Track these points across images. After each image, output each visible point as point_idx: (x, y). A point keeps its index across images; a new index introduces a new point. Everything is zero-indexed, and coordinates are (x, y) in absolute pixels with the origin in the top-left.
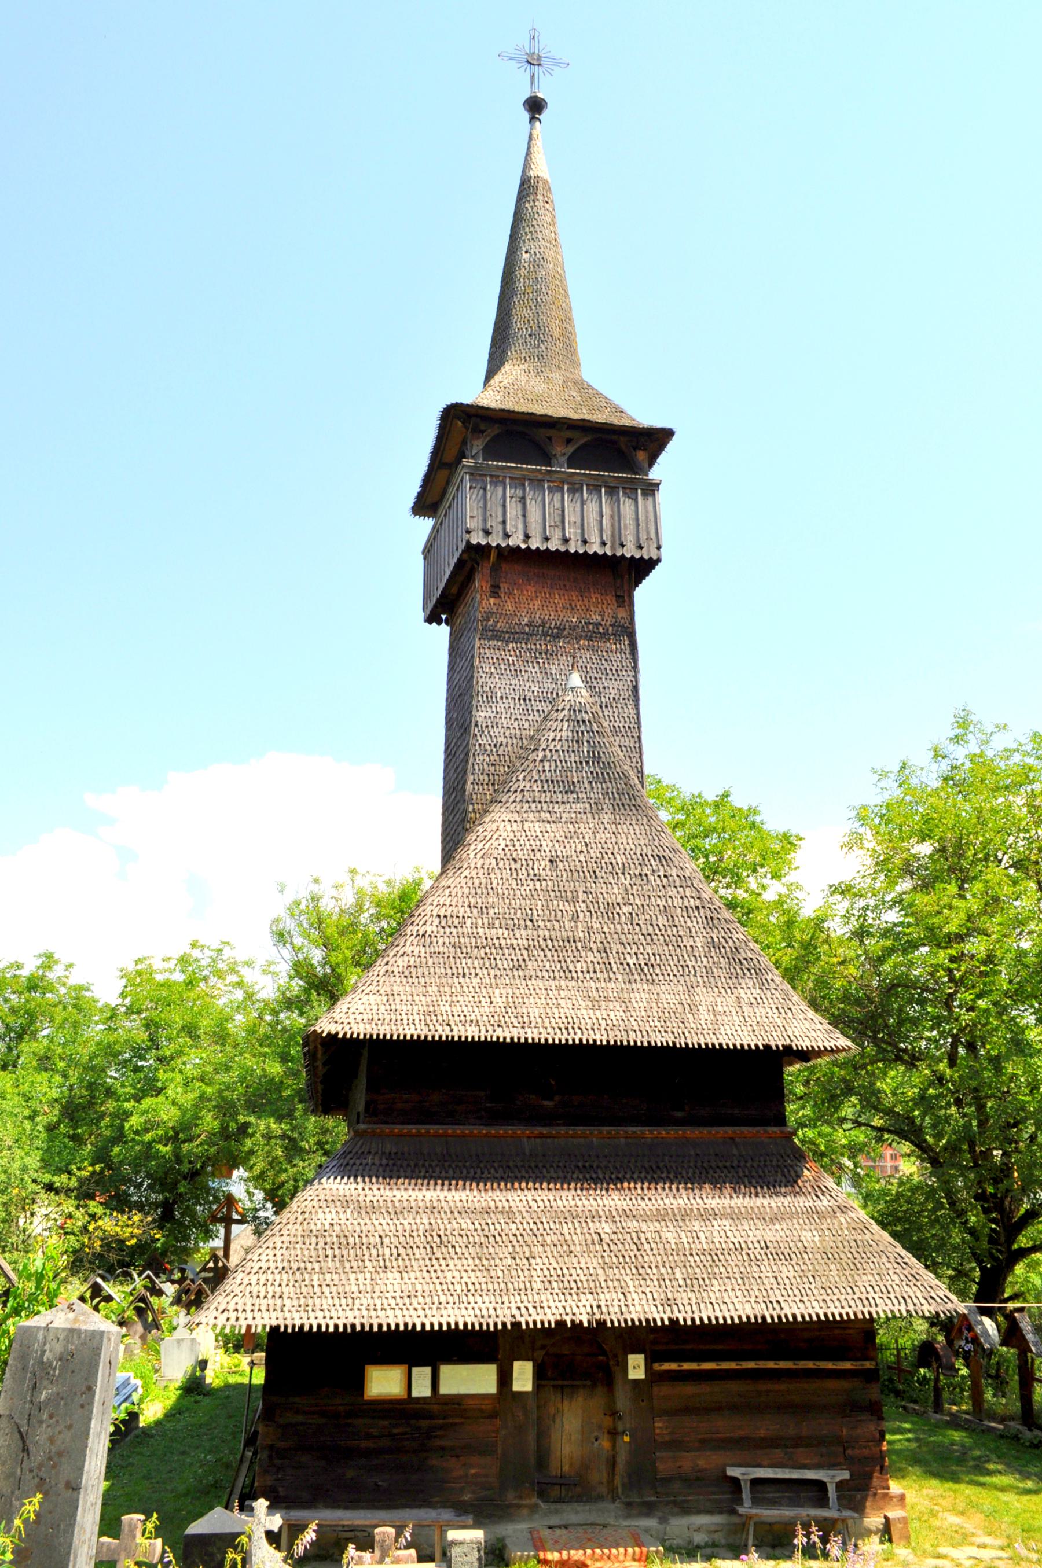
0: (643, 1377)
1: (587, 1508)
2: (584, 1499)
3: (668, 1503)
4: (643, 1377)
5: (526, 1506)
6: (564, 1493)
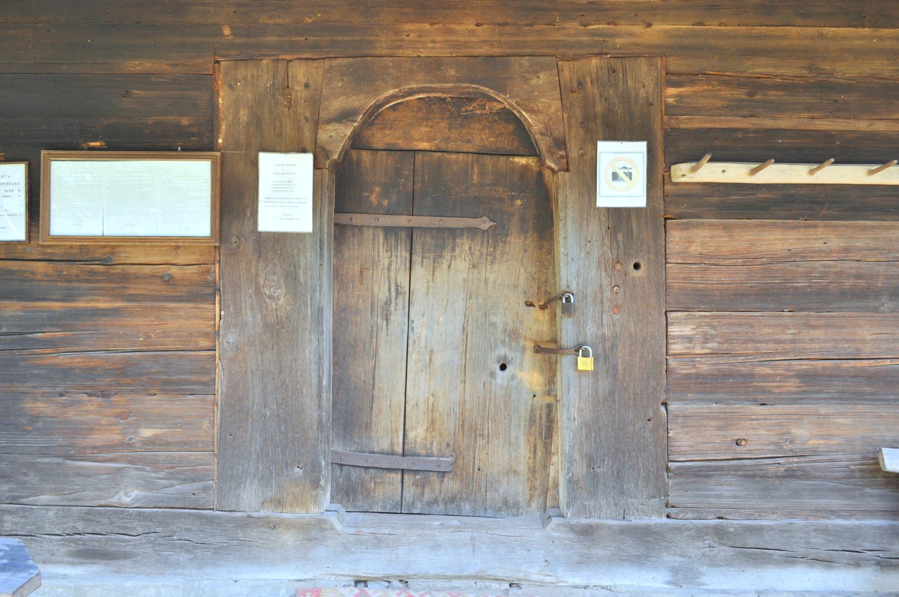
0: (641, 202)
1: (466, 536)
2: (466, 507)
3: (700, 533)
4: (641, 202)
5: (289, 525)
6: (410, 492)
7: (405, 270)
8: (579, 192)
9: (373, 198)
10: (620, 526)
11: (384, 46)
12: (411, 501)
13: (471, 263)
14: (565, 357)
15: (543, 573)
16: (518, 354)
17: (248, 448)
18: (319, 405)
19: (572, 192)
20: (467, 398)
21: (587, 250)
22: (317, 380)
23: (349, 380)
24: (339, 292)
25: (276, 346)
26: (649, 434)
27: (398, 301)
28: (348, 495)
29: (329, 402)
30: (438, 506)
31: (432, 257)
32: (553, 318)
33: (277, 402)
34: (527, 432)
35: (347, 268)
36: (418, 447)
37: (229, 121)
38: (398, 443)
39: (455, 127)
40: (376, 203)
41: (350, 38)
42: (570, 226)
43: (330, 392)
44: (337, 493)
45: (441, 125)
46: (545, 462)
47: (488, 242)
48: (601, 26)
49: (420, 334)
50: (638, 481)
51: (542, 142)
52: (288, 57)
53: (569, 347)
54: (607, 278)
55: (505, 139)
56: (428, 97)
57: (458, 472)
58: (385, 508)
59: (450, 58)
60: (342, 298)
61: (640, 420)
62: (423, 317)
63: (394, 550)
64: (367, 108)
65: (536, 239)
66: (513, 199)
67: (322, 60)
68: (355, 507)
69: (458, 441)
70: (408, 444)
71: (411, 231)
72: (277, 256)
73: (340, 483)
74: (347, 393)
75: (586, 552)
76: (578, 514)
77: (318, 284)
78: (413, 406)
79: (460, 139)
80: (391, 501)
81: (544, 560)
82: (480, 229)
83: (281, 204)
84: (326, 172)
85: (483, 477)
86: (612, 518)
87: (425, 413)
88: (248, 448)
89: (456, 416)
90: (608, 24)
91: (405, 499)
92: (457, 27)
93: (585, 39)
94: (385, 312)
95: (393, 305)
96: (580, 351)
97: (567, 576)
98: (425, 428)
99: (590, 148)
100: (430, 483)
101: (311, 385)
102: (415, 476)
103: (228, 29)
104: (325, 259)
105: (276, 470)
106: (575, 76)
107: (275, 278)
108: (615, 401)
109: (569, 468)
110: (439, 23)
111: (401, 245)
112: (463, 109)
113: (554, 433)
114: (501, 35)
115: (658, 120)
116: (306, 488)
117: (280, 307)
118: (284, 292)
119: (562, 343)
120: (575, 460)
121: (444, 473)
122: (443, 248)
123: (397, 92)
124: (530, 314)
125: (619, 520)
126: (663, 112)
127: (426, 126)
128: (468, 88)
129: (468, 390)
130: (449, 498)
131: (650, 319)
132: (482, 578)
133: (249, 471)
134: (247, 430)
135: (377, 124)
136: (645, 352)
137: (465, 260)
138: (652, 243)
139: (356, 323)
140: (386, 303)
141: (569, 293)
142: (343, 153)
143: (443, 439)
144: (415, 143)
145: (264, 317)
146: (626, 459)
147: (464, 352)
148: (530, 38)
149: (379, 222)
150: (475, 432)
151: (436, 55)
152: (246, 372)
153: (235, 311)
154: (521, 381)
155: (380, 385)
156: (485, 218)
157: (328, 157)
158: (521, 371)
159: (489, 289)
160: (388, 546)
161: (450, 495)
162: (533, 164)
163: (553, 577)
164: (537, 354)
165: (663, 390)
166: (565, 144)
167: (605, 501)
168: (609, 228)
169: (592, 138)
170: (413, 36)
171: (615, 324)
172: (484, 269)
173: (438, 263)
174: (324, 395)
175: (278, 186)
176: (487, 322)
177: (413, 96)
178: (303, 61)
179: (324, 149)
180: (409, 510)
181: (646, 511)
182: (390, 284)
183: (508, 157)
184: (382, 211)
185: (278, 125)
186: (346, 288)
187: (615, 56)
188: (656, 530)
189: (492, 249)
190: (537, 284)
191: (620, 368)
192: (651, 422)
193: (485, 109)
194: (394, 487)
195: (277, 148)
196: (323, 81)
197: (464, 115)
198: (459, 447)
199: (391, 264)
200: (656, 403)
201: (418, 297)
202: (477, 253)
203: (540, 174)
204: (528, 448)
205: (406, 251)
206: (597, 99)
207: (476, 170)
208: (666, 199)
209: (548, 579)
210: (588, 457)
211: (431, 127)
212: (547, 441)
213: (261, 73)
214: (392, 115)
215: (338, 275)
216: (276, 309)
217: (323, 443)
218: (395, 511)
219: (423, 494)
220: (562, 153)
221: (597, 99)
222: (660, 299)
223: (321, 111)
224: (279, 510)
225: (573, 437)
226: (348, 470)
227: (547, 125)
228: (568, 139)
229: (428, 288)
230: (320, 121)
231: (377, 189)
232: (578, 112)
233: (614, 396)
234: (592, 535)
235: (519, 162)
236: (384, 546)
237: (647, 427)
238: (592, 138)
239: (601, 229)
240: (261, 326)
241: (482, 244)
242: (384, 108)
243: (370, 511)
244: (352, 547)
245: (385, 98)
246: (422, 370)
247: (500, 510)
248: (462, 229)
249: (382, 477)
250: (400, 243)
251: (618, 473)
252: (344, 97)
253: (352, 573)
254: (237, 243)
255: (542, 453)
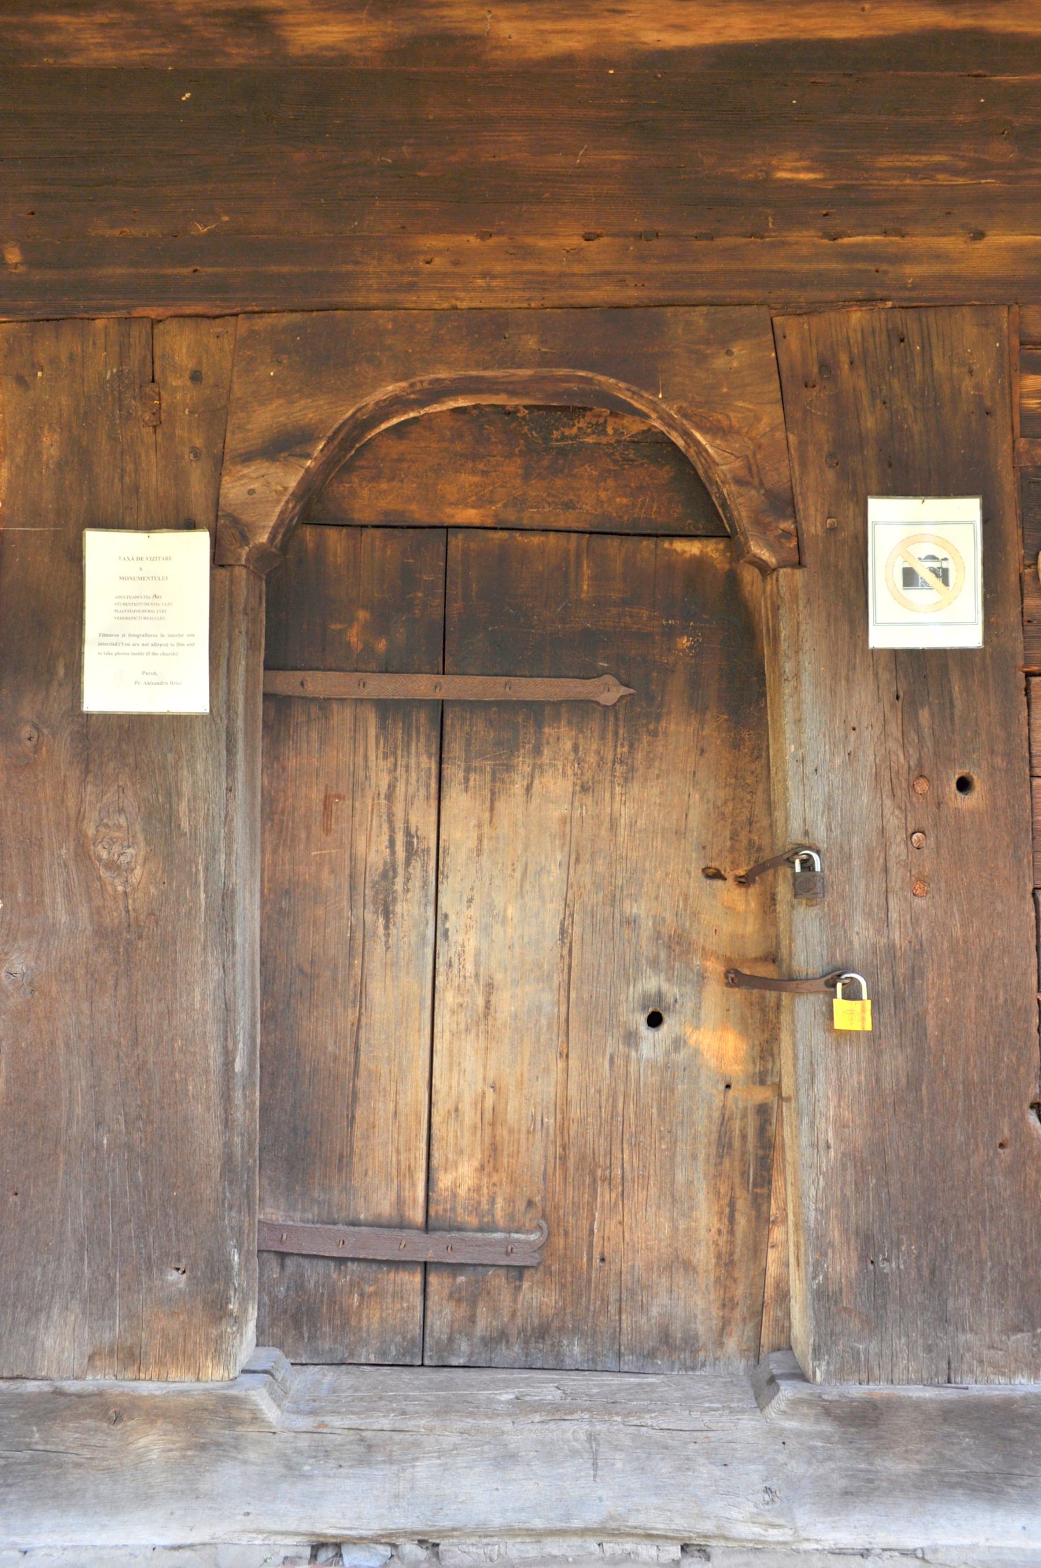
2: (575, 1350)
7: (428, 798)
8: (829, 615)
9: (354, 636)
10: (942, 1402)
11: (375, 286)
12: (444, 1337)
13: (578, 781)
14: (803, 998)
15: (761, 1520)
16: (688, 989)
17: (57, 1225)
18: (227, 1119)
19: (811, 615)
20: (573, 1091)
21: (850, 749)
22: (220, 1060)
23: (299, 1054)
24: (275, 851)
25: (123, 981)
26: (1002, 1179)
27: (411, 870)
28: (297, 1324)
29: (252, 1111)
30: (508, 1348)
31: (488, 769)
32: (770, 902)
33: (126, 1115)
34: (712, 1171)
35: (294, 796)
36: (460, 1210)
37: (18, 460)
38: (414, 1201)
39: (539, 474)
40: (360, 646)
41: (296, 269)
42: (808, 693)
43: (254, 1084)
44: (273, 1319)
45: (505, 469)
46: (755, 1241)
47: (616, 733)
48: (869, 239)
49: (463, 946)
50: (979, 1292)
51: (740, 500)
52: (153, 312)
53: (810, 976)
54: (897, 812)
55: (653, 500)
56: (476, 407)
57: (555, 1267)
58: (384, 1353)
59: (526, 311)
60: (283, 864)
61: (981, 1145)
62: (469, 907)
63: (404, 1470)
64: (336, 426)
65: (725, 726)
66: (670, 633)
67: (232, 319)
68: (316, 1352)
69: (554, 1193)
70: (438, 1203)
71: (440, 710)
72: (127, 769)
73: (281, 1297)
74: (295, 1085)
75: (863, 1466)
76: (840, 1374)
77: (222, 834)
78: (449, 1112)
79: (550, 500)
80: (399, 1338)
81: (762, 1486)
82: (598, 703)
83: (136, 649)
84: (241, 573)
85: (612, 1278)
86: (921, 1381)
87: (476, 1127)
88: (57, 1225)
89: (547, 1135)
90: (885, 233)
91: (432, 1331)
92: (542, 243)
93: (834, 266)
94: (381, 897)
95: (399, 880)
96: (839, 986)
97: (819, 1526)
98: (476, 1163)
99: (851, 514)
100: (489, 1293)
101: (206, 1072)
102: (455, 1277)
103: (16, 250)
104: (240, 775)
105: (122, 1276)
106: (815, 351)
107: (122, 821)
108: (922, 1101)
109: (817, 1264)
110: (500, 233)
111: (418, 740)
112: (556, 434)
113: (775, 1176)
114: (642, 258)
115: (1006, 447)
116: (195, 1320)
117: (135, 890)
118: (142, 853)
119: (795, 966)
120: (831, 1244)
121: (521, 1270)
122: (513, 748)
123: (403, 389)
124: (714, 896)
125: (938, 1385)
126: (1017, 430)
127: (473, 472)
128: (567, 379)
129: (574, 1073)
130: (533, 1329)
131: (999, 907)
132: (616, 1534)
133: (60, 1281)
134: (56, 1181)
135: (362, 467)
136: (989, 985)
137: (564, 774)
138: (999, 731)
139: (315, 922)
140: (384, 875)
141: (810, 848)
142: (282, 530)
143: (518, 1190)
144: (449, 510)
145: (97, 913)
146: (951, 1238)
147: (564, 986)
148: (708, 266)
149: (366, 690)
150: (593, 1173)
151: (493, 305)
152: (52, 1043)
153: (29, 899)
154: (697, 1052)
155: (372, 1066)
156: (608, 679)
157: (244, 539)
158: (697, 1028)
159: (620, 839)
160: (391, 1462)
161: (536, 1321)
162: (715, 555)
163: (786, 1530)
164: (731, 990)
165: (1033, 1075)
166: (792, 503)
167: (903, 1341)
168: (898, 698)
169: (855, 491)
170: (439, 263)
171: (917, 920)
172: (608, 795)
173: (503, 782)
174: (238, 1095)
175: (129, 607)
176: (617, 916)
177: (443, 402)
178: (187, 320)
179: (235, 521)
180: (440, 1357)
181: (1002, 1363)
182: (392, 830)
183: (659, 540)
184: (373, 666)
185: (130, 467)
186: (292, 841)
187: (904, 304)
188: (1027, 1411)
189: (625, 749)
190: (729, 827)
191: (931, 1023)
192: (1007, 1151)
193: (606, 434)
194: (405, 1305)
195: (128, 519)
196: (233, 366)
197: (558, 448)
198: (557, 1208)
199: (395, 787)
200: (1016, 1104)
201: (457, 859)
202: (592, 759)
203: (733, 579)
204: (716, 1208)
205: (430, 757)
206: (865, 400)
207: (586, 571)
208: (1029, 628)
209: (774, 1535)
210: (862, 1235)
211: (485, 473)
212: (758, 1191)
213: (90, 349)
214: (396, 448)
215: (272, 813)
216: (125, 893)
217: (235, 1209)
218: (408, 1361)
219: (472, 1319)
220: (787, 525)
221: (865, 400)
222: (1020, 861)
223: (228, 434)
224: (129, 1375)
225: (824, 1189)
226: (298, 1266)
227: (752, 461)
228: (801, 494)
229: (480, 839)
230: (226, 458)
231: (362, 615)
232: (822, 432)
233: (918, 1090)
234: (876, 1426)
235: (684, 552)
236: (380, 1459)
237: (997, 1162)
238: (855, 491)
239: (879, 700)
240: (88, 933)
241: (603, 738)
242: (377, 431)
243: (350, 1361)
244: (305, 1464)
245: (377, 403)
246: (467, 1030)
247: (652, 1354)
248: (556, 705)
249: (376, 1281)
250: (414, 738)
251: (933, 1273)
252: (281, 401)
253: (305, 1527)
254: (34, 740)
255: (749, 1221)
